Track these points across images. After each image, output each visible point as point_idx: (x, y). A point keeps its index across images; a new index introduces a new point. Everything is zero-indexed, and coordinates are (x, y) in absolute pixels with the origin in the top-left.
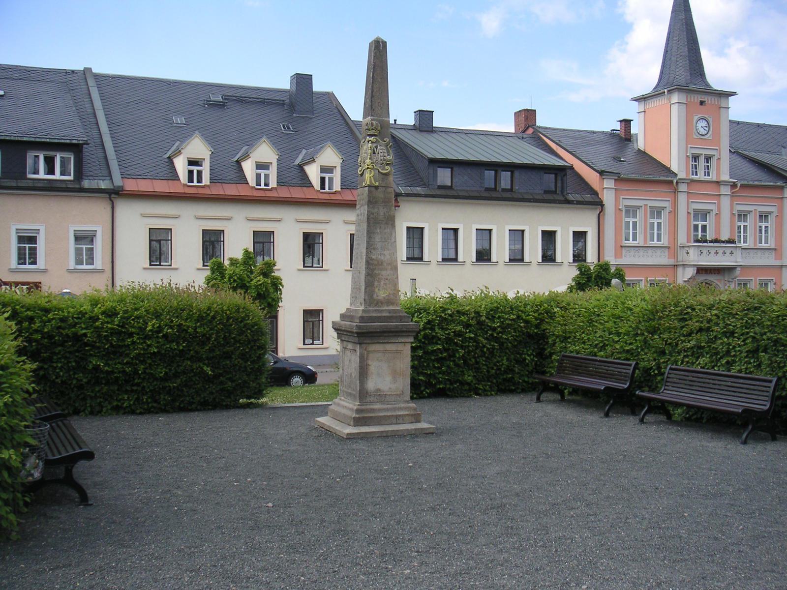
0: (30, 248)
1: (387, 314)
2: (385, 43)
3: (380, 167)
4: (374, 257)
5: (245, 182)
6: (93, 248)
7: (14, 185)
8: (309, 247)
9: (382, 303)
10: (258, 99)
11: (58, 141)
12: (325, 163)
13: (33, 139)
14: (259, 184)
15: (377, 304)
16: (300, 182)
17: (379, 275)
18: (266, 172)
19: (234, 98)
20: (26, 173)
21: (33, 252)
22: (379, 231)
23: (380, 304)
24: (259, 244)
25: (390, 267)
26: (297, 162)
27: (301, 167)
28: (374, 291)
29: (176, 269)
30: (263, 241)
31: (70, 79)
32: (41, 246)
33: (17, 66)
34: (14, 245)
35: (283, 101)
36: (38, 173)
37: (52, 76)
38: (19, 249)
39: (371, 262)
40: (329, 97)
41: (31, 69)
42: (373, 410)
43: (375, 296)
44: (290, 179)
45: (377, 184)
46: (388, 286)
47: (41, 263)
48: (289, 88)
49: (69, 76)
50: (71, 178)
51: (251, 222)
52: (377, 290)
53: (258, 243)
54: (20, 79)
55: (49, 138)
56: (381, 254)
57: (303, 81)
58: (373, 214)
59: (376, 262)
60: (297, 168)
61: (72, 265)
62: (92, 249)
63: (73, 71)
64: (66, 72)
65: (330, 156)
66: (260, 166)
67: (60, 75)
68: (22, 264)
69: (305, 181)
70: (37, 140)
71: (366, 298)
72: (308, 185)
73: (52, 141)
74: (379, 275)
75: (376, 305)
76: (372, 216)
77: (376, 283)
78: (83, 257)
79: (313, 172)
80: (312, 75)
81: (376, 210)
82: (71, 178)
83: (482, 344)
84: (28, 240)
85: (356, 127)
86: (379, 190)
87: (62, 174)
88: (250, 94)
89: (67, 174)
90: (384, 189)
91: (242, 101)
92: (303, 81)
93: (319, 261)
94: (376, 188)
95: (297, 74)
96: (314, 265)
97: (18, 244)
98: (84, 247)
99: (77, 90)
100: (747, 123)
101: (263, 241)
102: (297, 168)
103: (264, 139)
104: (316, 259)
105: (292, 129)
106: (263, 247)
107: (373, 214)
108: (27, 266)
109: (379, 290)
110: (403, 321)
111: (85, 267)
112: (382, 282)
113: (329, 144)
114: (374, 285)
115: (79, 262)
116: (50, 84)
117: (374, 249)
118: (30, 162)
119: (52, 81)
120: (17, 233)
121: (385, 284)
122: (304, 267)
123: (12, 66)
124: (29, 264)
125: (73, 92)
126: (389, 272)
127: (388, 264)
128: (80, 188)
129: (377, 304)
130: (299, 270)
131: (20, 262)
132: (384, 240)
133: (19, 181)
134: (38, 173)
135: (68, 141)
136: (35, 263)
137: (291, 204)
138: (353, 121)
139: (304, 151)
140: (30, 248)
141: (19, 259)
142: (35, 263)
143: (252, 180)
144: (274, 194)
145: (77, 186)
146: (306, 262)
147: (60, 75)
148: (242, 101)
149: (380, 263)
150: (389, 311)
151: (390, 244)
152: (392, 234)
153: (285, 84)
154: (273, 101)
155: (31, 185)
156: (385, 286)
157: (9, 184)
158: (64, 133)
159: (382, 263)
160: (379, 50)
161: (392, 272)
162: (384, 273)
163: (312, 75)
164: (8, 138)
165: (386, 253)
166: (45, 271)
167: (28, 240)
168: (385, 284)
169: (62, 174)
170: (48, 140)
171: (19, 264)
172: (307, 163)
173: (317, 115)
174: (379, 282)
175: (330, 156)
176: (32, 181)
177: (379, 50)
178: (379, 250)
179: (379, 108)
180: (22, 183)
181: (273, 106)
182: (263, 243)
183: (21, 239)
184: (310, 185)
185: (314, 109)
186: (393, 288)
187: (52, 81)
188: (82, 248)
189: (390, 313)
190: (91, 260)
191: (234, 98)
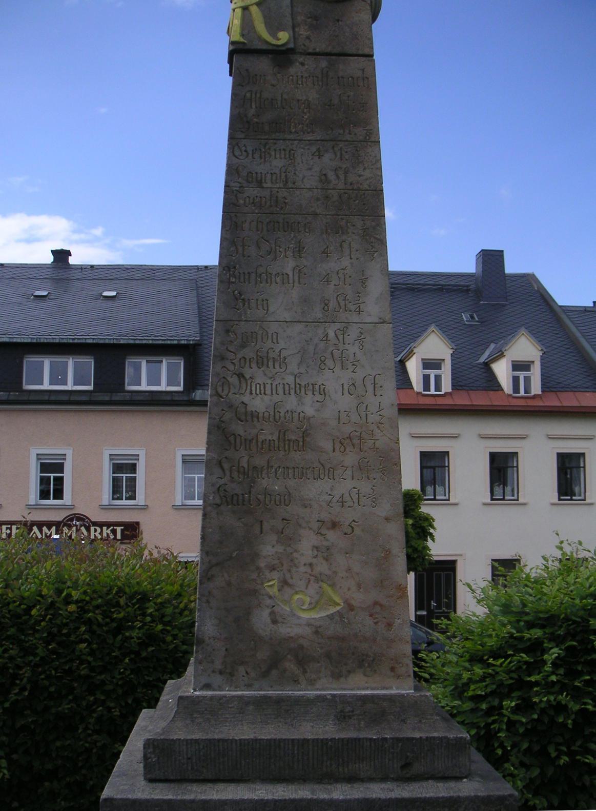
0: (55, 478)
1: (328, 730)
4: (258, 404)
5: (410, 387)
6: (113, 473)
7: (107, 398)
8: (499, 470)
9: (303, 659)
10: (434, 285)
11: (163, 342)
12: (518, 359)
13: (132, 342)
14: (426, 386)
15: (275, 662)
16: (485, 385)
17: (287, 498)
18: (437, 372)
19: (404, 286)
20: (124, 384)
21: (132, 482)
22: (289, 265)
23: (291, 666)
24: (440, 469)
25: (351, 459)
26: (482, 360)
27: (487, 366)
28: (254, 593)
29: (525, 504)
31: (201, 276)
32: (67, 475)
33: (142, 266)
35: (467, 286)
37: (180, 274)
38: (42, 479)
39: (239, 429)
40: (528, 282)
41: (158, 268)
43: (261, 621)
44: (472, 381)
45: (284, 37)
47: (140, 499)
48: (474, 272)
49: (201, 272)
50: (181, 388)
51: (416, 439)
52: (271, 586)
53: (427, 467)
54: (142, 279)
55: (152, 340)
56: (298, 390)
57: (491, 260)
58: (260, 183)
59: (268, 433)
60: (482, 367)
62: (62, 479)
63: (206, 267)
64: (198, 268)
65: (524, 348)
66: (429, 364)
67: (190, 272)
68: (118, 499)
69: (492, 383)
70: (137, 342)
72: (496, 388)
73: (155, 342)
74: (287, 498)
75: (272, 667)
76: (252, 192)
77: (269, 549)
78: (195, 490)
79: (502, 370)
80: (502, 251)
81: (278, 163)
82: (181, 388)
85: (565, 313)
88: (425, 280)
90: (324, 63)
91: (412, 290)
92: (491, 260)
93: (513, 490)
94: (282, 56)
95: (482, 250)
96: (507, 498)
97: (114, 473)
98: (196, 476)
99: (207, 288)
102: (482, 367)
103: (432, 328)
104: (508, 489)
105: (477, 319)
106: (434, 474)
107: (260, 183)
108: (124, 502)
109: (284, 583)
110: (417, 768)
111: (52, 502)
112: (307, 543)
113: (523, 331)
114: (256, 556)
116: (177, 283)
117: (262, 361)
118: (129, 371)
119: (180, 279)
120: (111, 459)
121: (325, 552)
122: (492, 499)
123: (136, 265)
124: (127, 499)
125: (203, 289)
126: (345, 486)
127: (344, 442)
128: (189, 401)
129: (275, 662)
130: (485, 504)
131: (115, 497)
132: (318, 314)
133: (114, 394)
135: (175, 342)
136: (133, 497)
138: (561, 306)
139: (492, 346)
140: (55, 478)
141: (114, 492)
142: (133, 497)
143: (418, 383)
144: (448, 401)
145: (186, 398)
146: (495, 493)
147: (190, 272)
148: (412, 290)
149: (295, 437)
150: (344, 710)
151: (353, 332)
152: (363, 282)
153: (467, 265)
154: (455, 288)
155: (128, 398)
156: (322, 567)
157: (100, 398)
158: (173, 333)
159: (305, 434)
161: (365, 487)
162: (315, 490)
163: (502, 251)
164: (102, 342)
165: (333, 380)
166: (145, 508)
168: (325, 552)
169: (169, 384)
170: (151, 342)
171: (113, 499)
172: (495, 360)
173: (511, 301)
174: (288, 539)
175: (524, 348)
176: (130, 394)
178: (293, 366)
180: (118, 397)
181: (453, 293)
182: (434, 468)
183: (45, 467)
184: (499, 388)
185: (508, 294)
187: (180, 279)
188: (195, 477)
189: (343, 717)
190: (59, 494)
191: (404, 286)
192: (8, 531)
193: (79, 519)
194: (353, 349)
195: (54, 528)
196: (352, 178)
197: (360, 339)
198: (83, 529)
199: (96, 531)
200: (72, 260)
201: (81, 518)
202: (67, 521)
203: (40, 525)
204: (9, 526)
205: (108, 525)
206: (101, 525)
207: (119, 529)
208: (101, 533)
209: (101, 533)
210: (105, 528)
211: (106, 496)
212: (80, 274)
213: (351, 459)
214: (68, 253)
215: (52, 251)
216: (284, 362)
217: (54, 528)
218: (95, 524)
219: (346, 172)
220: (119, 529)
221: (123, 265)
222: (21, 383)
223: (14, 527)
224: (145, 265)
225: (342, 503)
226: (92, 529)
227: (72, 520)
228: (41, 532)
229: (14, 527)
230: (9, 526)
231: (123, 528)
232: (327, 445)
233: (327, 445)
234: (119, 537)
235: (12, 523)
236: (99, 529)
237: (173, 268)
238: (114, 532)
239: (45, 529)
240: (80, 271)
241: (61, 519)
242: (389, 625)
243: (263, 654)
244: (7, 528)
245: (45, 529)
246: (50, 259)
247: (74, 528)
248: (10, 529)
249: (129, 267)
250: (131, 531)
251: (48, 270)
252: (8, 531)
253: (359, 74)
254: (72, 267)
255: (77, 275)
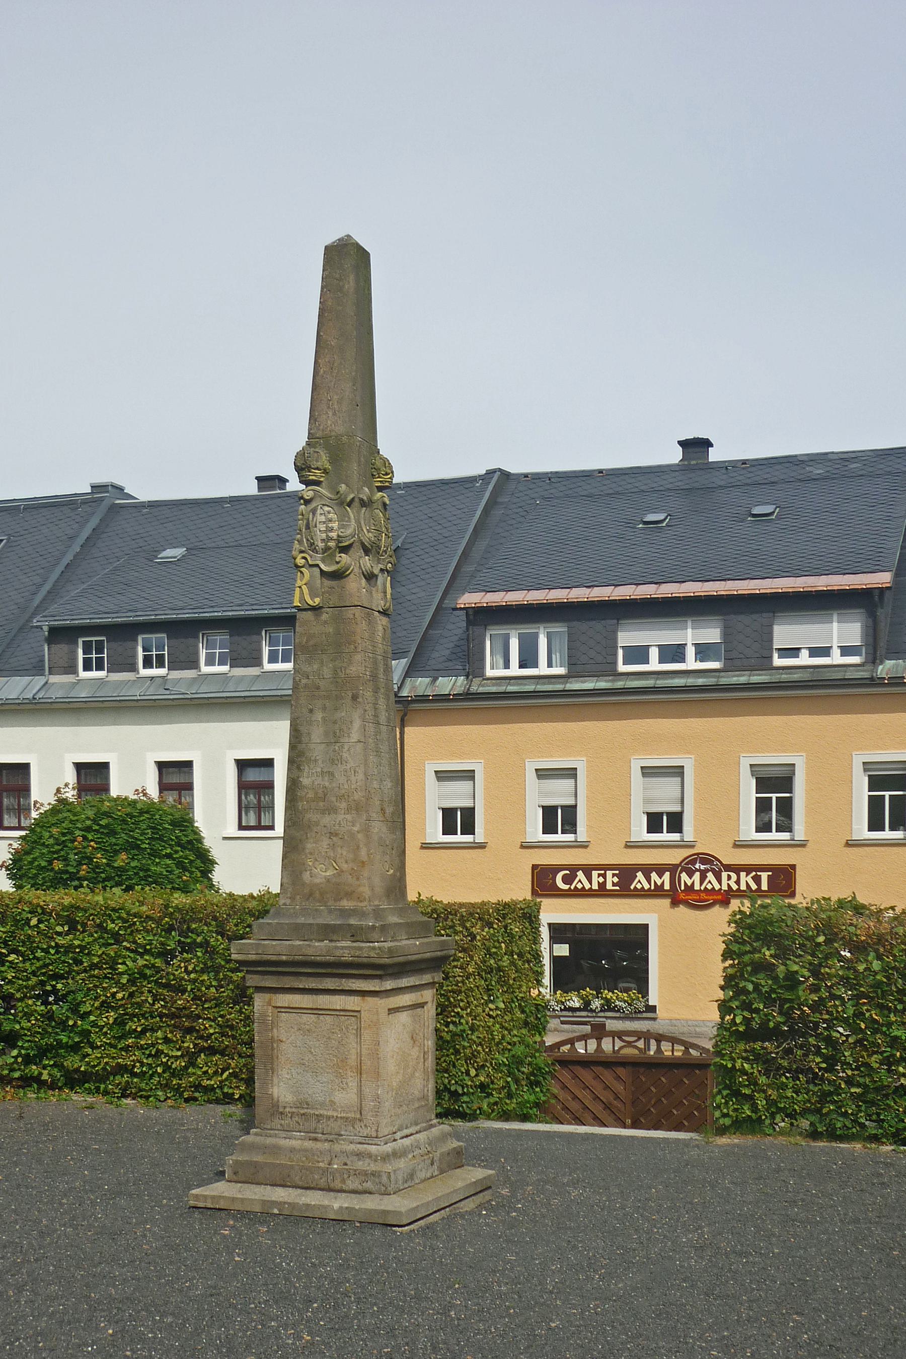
3: (323, 561)
21: (786, 807)
25: (343, 805)
30: (176, 775)
34: (749, 794)
36: (536, 665)
43: (306, 876)
45: (317, 600)
61: (862, 831)
74: (317, 824)
83: (884, 1143)
84: (775, 783)
86: (324, 617)
87: (522, 666)
101: (176, 775)
115: (763, 827)
120: (865, 770)
134: (536, 665)
137: (801, 609)
145: (866, 675)
160: (347, 266)
166: (802, 845)
167: (775, 783)
169: (522, 666)
177: (347, 266)
179: (330, 413)
190: (786, 826)
192: (601, 880)
194: (345, 755)
195: (668, 874)
196: (348, 671)
198: (710, 876)
199: (729, 878)
200: (715, 455)
201: (707, 859)
203: (647, 870)
205: (748, 869)
207: (764, 876)
208: (738, 882)
209: (738, 882)
210: (743, 874)
212: (724, 477)
213: (343, 805)
217: (668, 874)
218: (728, 868)
219: (345, 668)
220: (764, 876)
221: (796, 456)
222: (615, 663)
223: (609, 873)
224: (833, 453)
226: (724, 875)
227: (693, 862)
228: (649, 880)
229: (609, 873)
232: (334, 799)
233: (334, 799)
234: (764, 887)
235: (606, 868)
236: (734, 876)
237: (881, 453)
238: (757, 879)
239: (654, 876)
240: (724, 471)
242: (358, 879)
244: (599, 875)
245: (654, 876)
248: (604, 876)
250: (784, 879)
251: (674, 474)
252: (601, 880)
253: (352, 617)
254: (715, 466)
255: (719, 479)
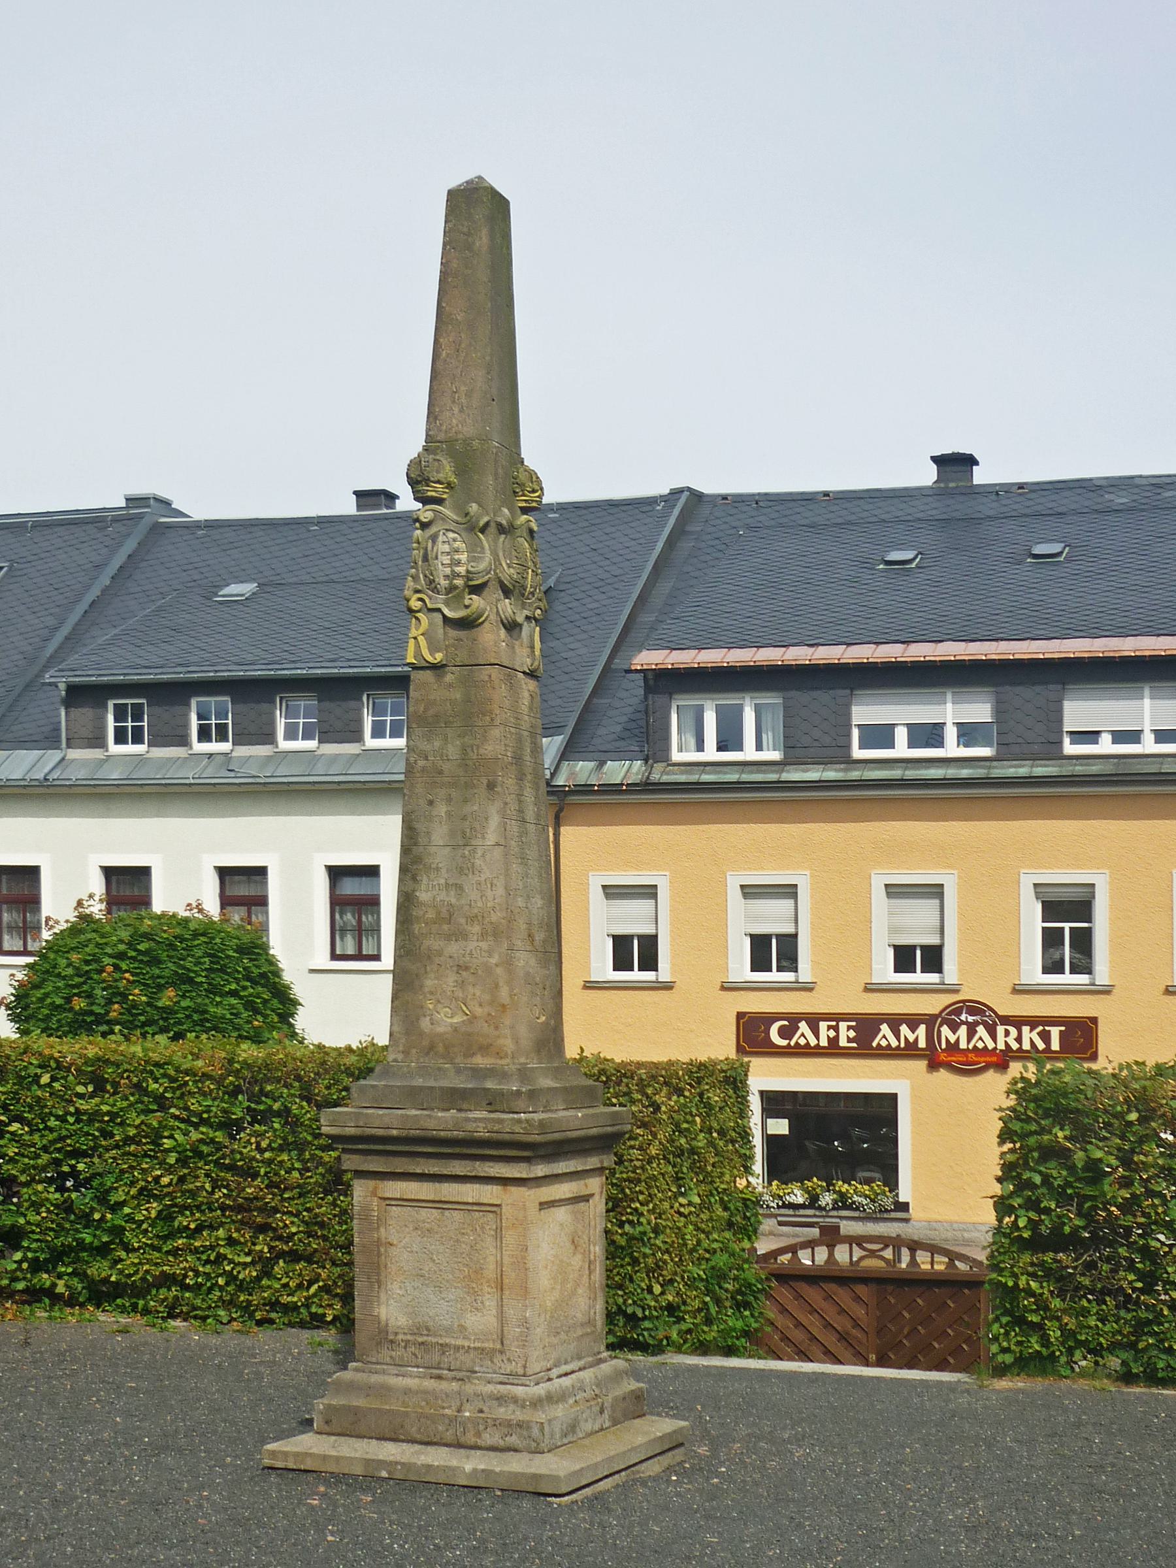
2: (499, 207)
3: (447, 603)
21: (1083, 942)
25: (476, 929)
33: (1132, 477)
42: (384, 1391)
43: (425, 1024)
45: (439, 656)
46: (471, 989)
47: (1103, 971)
62: (1088, 933)
71: (396, 1028)
84: (1068, 911)
86: (449, 678)
89: (650, 676)
100: (740, 500)
151: (480, 853)
160: (478, 221)
166: (1106, 991)
167: (1068, 911)
177: (478, 221)
179: (456, 410)
183: (1052, 909)
186: (487, 997)
188: (1063, 929)
192: (832, 1033)
193: (972, 1011)
194: (478, 862)
195: (922, 1028)
197: (483, 856)
199: (1007, 1033)
200: (981, 476)
201: (976, 1008)
202: (949, 1014)
203: (895, 1022)
204: (834, 1023)
205: (1033, 1022)
206: (1018, 1022)
207: (1055, 1032)
208: (1019, 1040)
209: (1019, 1040)
211: (1033, 972)
213: (476, 929)
214: (969, 461)
215: (932, 458)
216: (438, 869)
218: (1006, 1020)
220: (1055, 1032)
222: (848, 746)
223: (843, 1026)
224: (1141, 476)
225: (471, 954)
226: (1000, 1030)
227: (958, 1012)
228: (897, 1035)
229: (843, 1026)
230: (834, 1023)
231: (1063, 1028)
232: (463, 921)
233: (463, 921)
234: (1055, 1045)
235: (838, 1018)
236: (1013, 1032)
238: (1045, 1036)
239: (904, 1029)
240: (994, 497)
241: (936, 1012)
243: (425, 1043)
244: (829, 1028)
245: (904, 1029)
246: (928, 476)
247: (964, 1028)
249: (1104, 483)
250: (1081, 1036)
252: (832, 1033)
255: (988, 507)
